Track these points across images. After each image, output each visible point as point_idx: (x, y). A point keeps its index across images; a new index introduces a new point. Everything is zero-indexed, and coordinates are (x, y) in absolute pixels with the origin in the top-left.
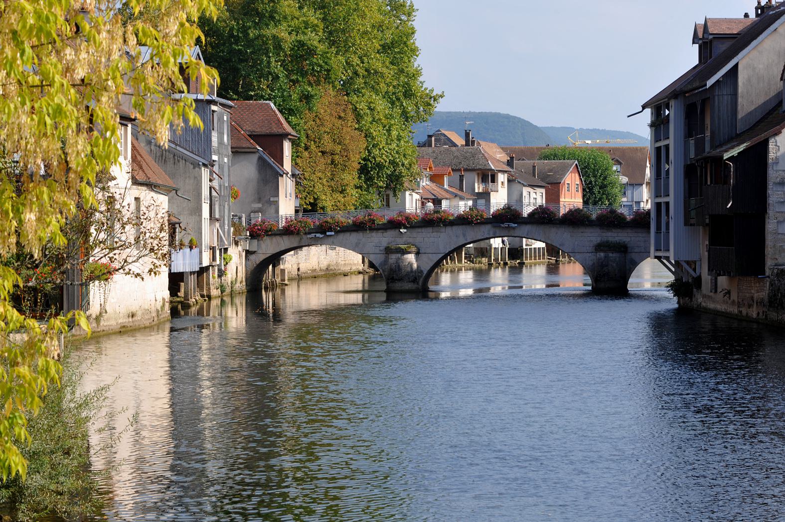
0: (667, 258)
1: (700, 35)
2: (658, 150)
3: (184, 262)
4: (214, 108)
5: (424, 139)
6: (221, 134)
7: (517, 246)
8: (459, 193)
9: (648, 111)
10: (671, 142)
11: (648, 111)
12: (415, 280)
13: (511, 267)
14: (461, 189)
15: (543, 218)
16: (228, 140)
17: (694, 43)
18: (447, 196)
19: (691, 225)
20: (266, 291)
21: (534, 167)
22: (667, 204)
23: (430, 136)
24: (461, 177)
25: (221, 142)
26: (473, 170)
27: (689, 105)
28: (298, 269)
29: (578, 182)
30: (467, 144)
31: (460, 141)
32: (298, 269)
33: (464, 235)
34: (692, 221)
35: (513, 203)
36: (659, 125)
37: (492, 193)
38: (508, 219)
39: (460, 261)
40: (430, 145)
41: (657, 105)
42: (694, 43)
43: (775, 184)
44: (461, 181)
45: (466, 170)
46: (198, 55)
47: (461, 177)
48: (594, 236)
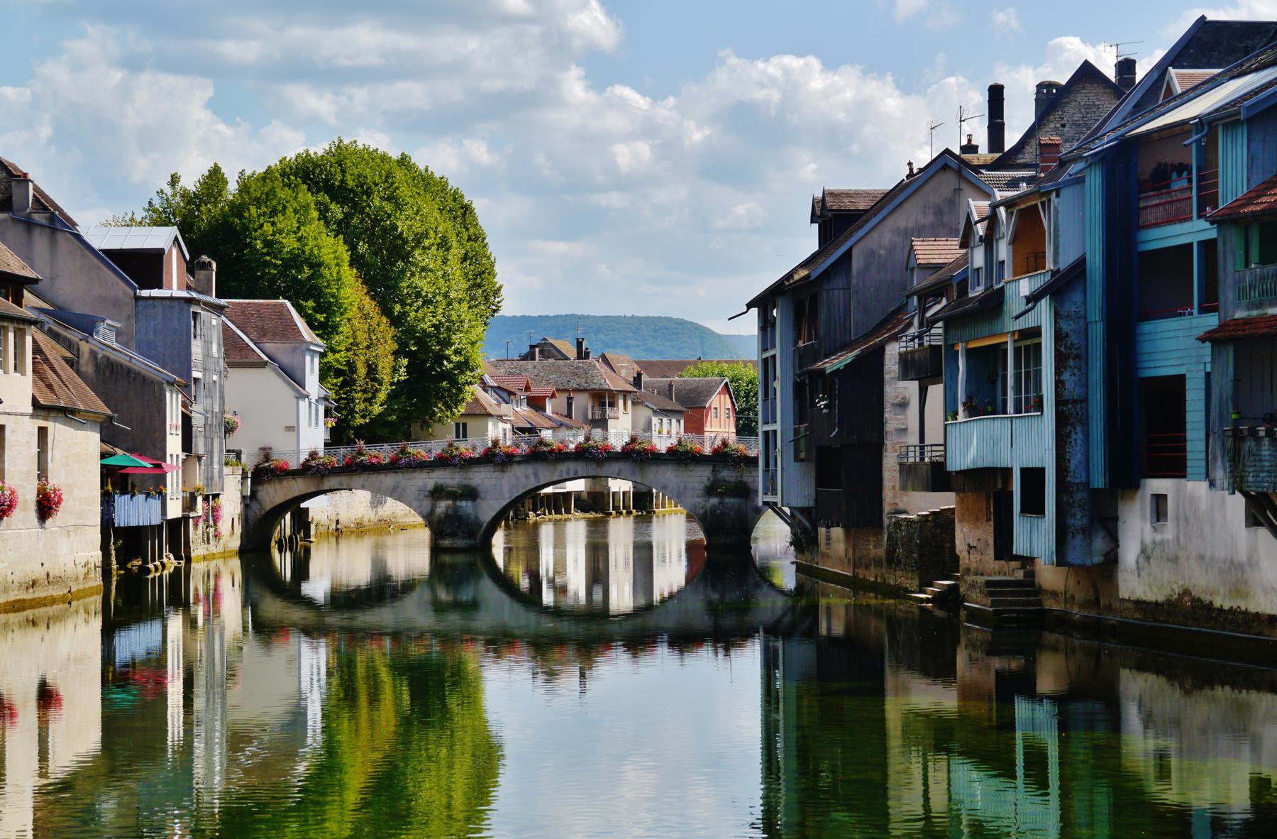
0: (776, 504)
1: (818, 212)
2: (765, 361)
3: (135, 511)
4: (194, 308)
5: (526, 350)
6: (208, 343)
7: (598, 489)
8: (566, 421)
9: (754, 311)
10: (776, 351)
11: (754, 311)
12: (471, 534)
13: (636, 517)
14: (569, 415)
15: (680, 457)
16: (219, 350)
17: (812, 222)
18: (550, 424)
19: (802, 460)
20: (280, 551)
21: (671, 386)
22: (775, 432)
23: (532, 347)
24: (570, 400)
25: (207, 355)
26: (585, 390)
27: (792, 304)
28: (337, 522)
29: (729, 406)
30: (579, 356)
31: (571, 352)
32: (337, 522)
33: (536, 475)
34: (803, 455)
35: (640, 432)
36: (766, 325)
37: (610, 422)
38: (636, 456)
39: (568, 512)
40: (533, 359)
41: (763, 303)
42: (812, 222)
43: (894, 405)
44: (570, 405)
45: (576, 390)
46: (176, 239)
47: (570, 400)
48: (702, 475)
